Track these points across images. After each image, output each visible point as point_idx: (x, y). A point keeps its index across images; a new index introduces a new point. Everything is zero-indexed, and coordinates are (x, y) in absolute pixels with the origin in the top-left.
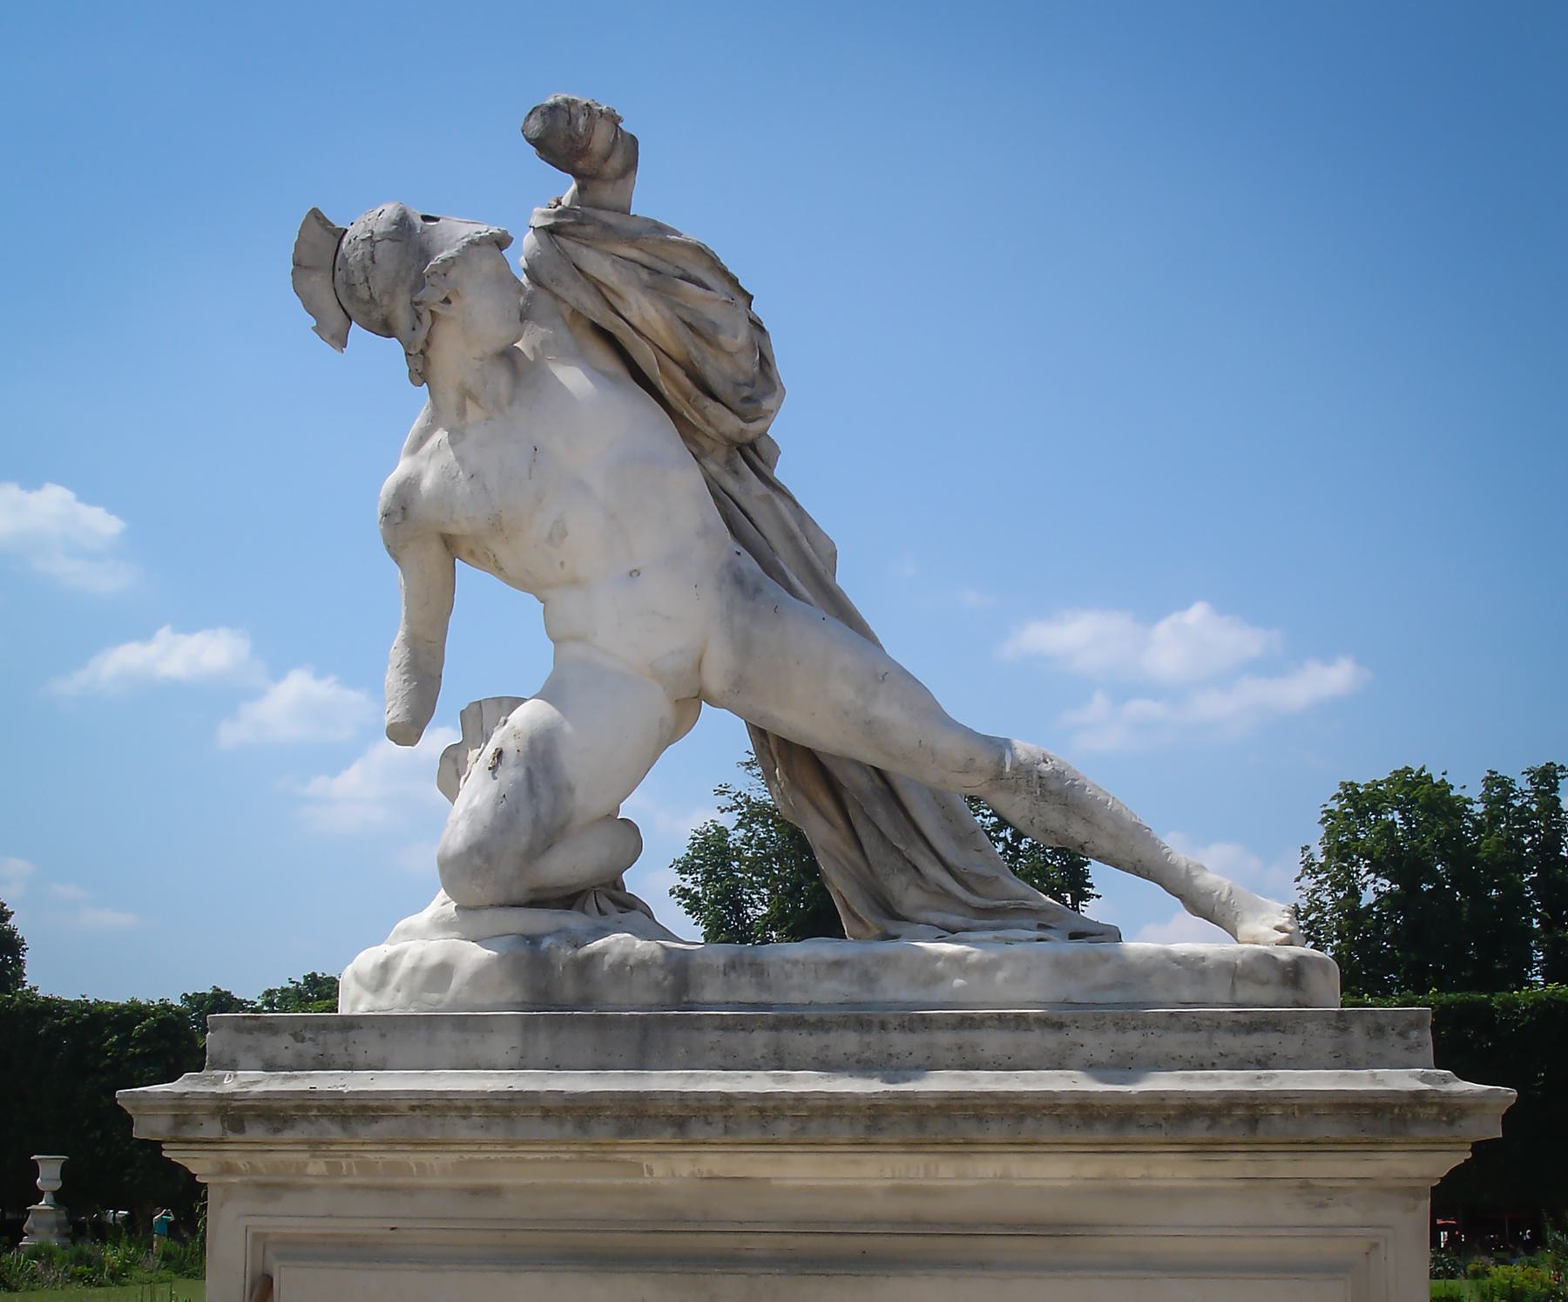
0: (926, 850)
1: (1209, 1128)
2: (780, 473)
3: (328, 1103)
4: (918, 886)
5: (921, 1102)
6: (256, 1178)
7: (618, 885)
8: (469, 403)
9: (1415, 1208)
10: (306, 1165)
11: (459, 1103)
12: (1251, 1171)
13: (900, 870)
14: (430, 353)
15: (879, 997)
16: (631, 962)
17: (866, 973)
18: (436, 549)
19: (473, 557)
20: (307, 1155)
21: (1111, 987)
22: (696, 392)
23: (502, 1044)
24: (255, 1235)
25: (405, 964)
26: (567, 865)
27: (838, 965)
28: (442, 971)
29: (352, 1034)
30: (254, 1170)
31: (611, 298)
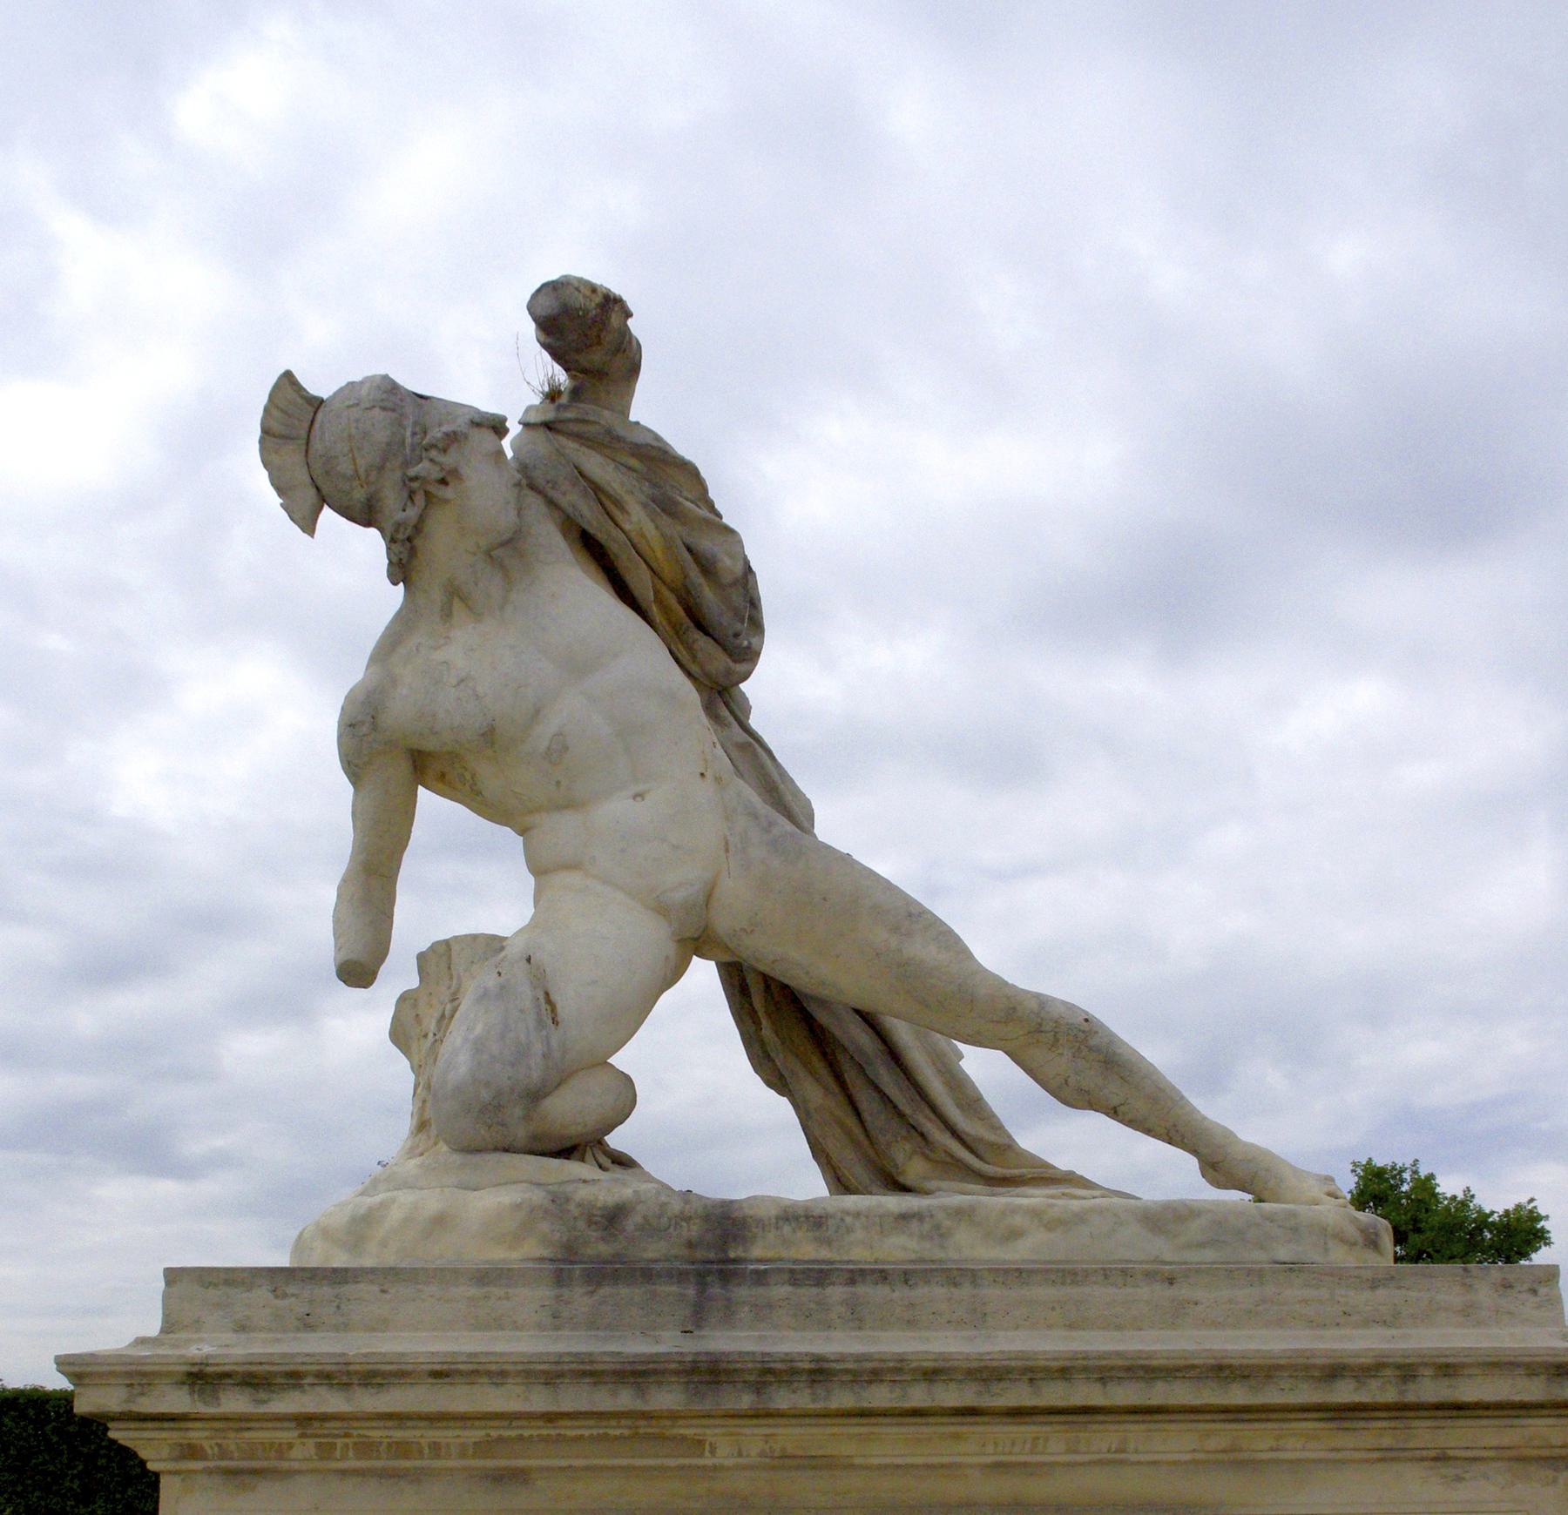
0: (932, 1115)
1: (1356, 1389)
2: (754, 722)
3: (328, 1368)
4: (923, 1154)
6: (224, 1464)
7: (601, 1143)
9: (1555, 1481)
10: (290, 1446)
11: (493, 1367)
13: (905, 1138)
14: (418, 542)
15: (953, 1255)
17: (938, 1227)
18: (405, 767)
20: (296, 1433)
21: (1202, 1245)
23: (532, 1298)
25: (396, 1215)
26: (568, 1109)
27: (904, 1217)
28: (440, 1221)
29: (347, 1289)
31: (608, 503)
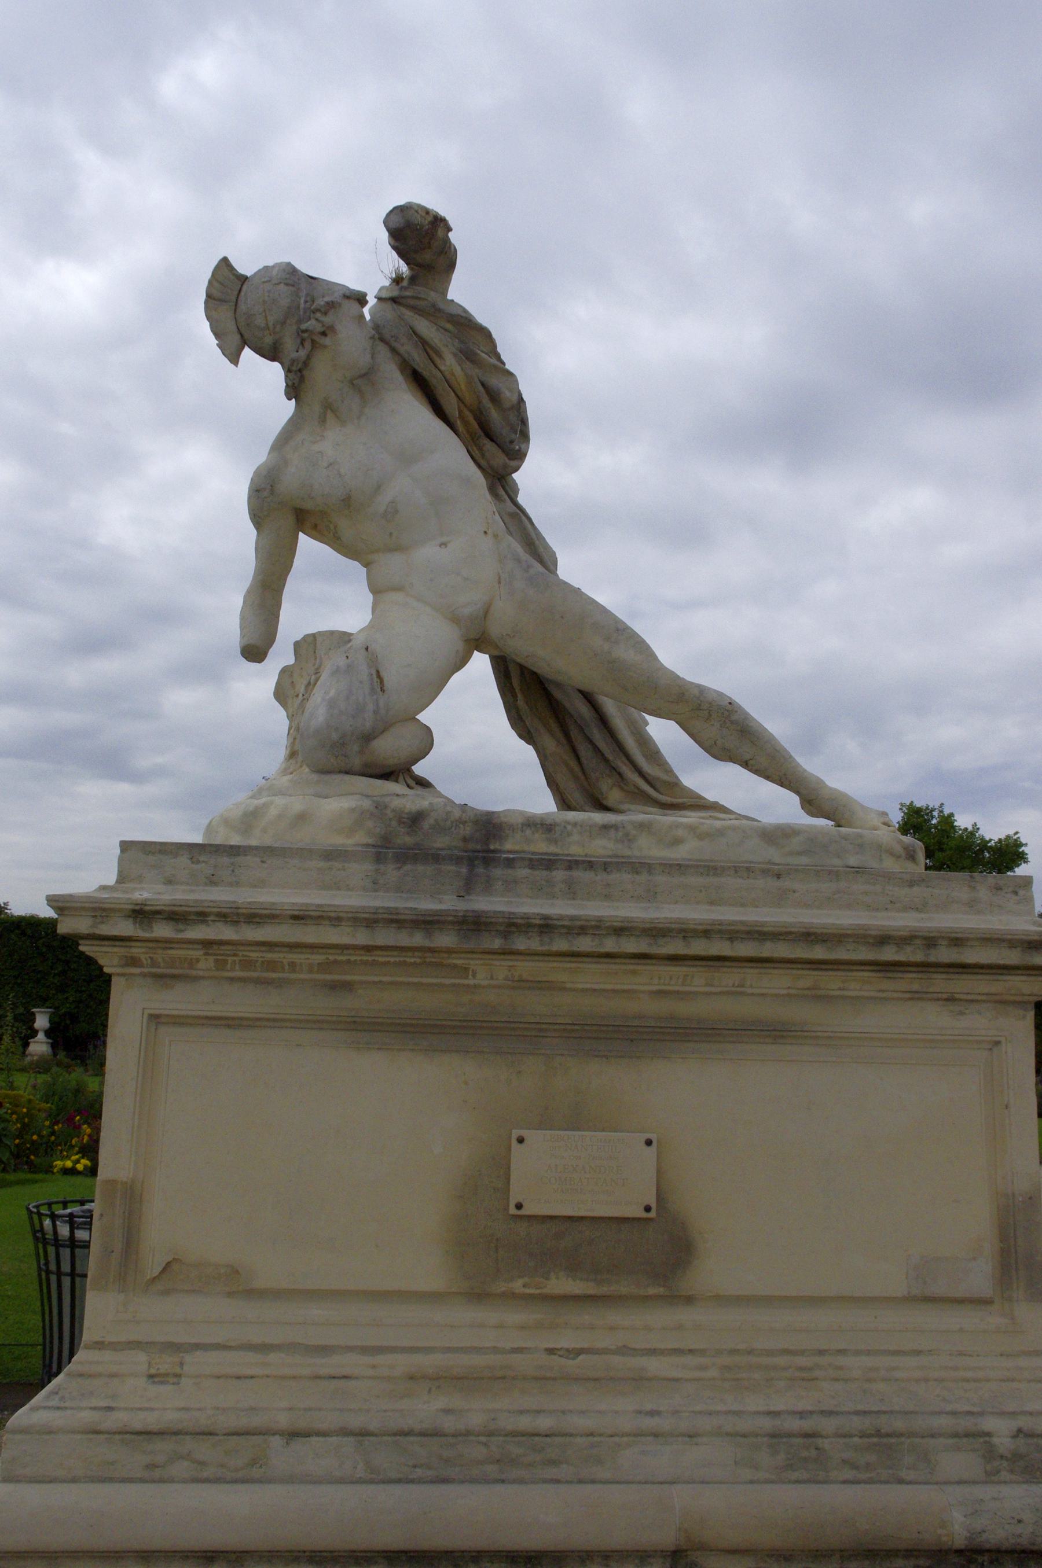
1: (897, 952)
5: (692, 926)
8: (329, 411)
9: (1024, 1017)
10: (198, 960)
11: (333, 915)
12: (916, 987)
14: (306, 373)
16: (734, 718)
17: (627, 835)
18: (291, 519)
19: (318, 533)
20: (201, 952)
22: (480, 432)
23: (359, 870)
24: (151, 1016)
25: (273, 812)
26: (389, 747)
27: (606, 827)
28: (302, 818)
29: (239, 859)
30: (154, 964)
